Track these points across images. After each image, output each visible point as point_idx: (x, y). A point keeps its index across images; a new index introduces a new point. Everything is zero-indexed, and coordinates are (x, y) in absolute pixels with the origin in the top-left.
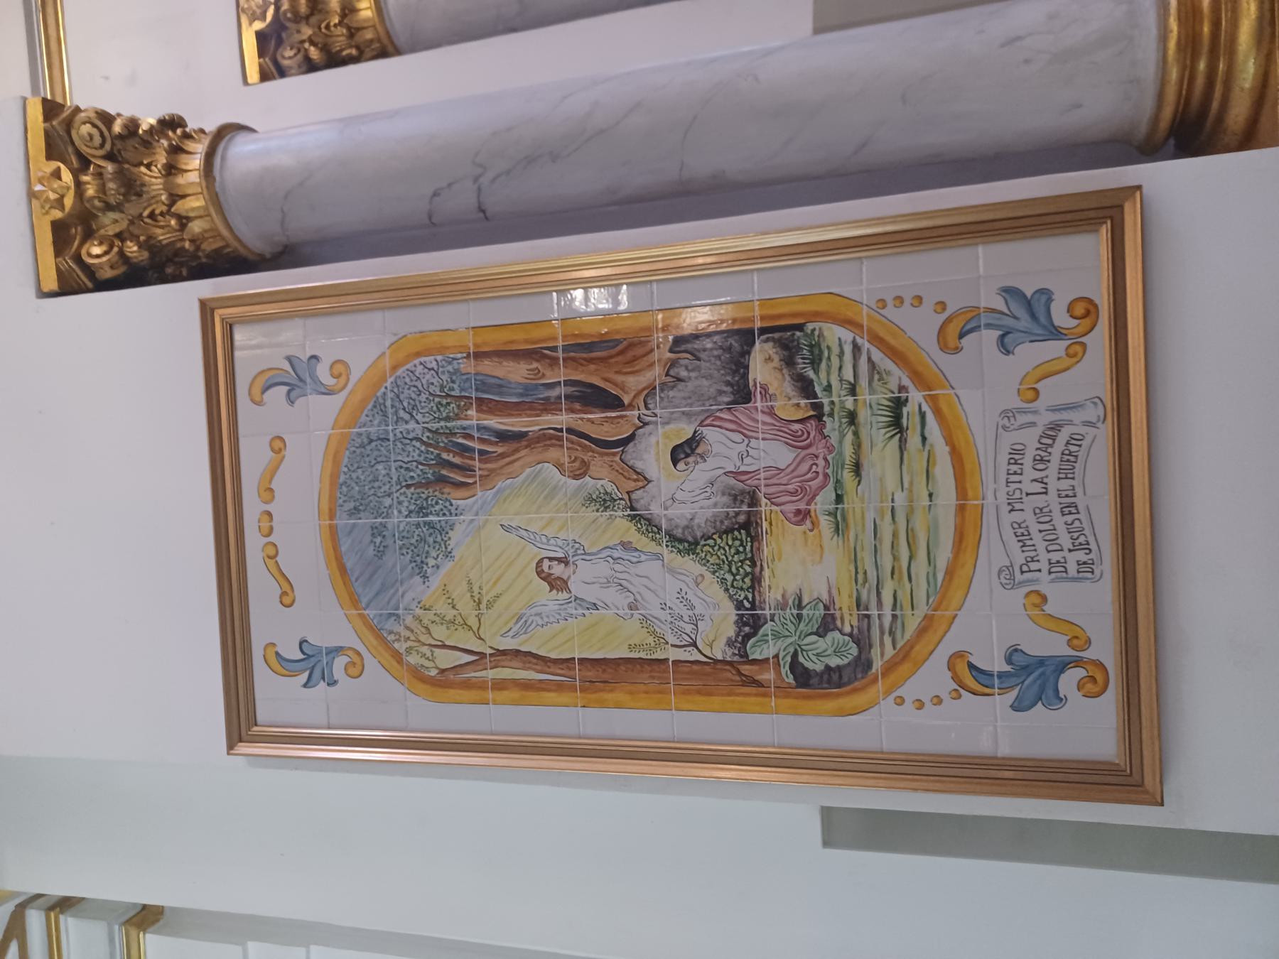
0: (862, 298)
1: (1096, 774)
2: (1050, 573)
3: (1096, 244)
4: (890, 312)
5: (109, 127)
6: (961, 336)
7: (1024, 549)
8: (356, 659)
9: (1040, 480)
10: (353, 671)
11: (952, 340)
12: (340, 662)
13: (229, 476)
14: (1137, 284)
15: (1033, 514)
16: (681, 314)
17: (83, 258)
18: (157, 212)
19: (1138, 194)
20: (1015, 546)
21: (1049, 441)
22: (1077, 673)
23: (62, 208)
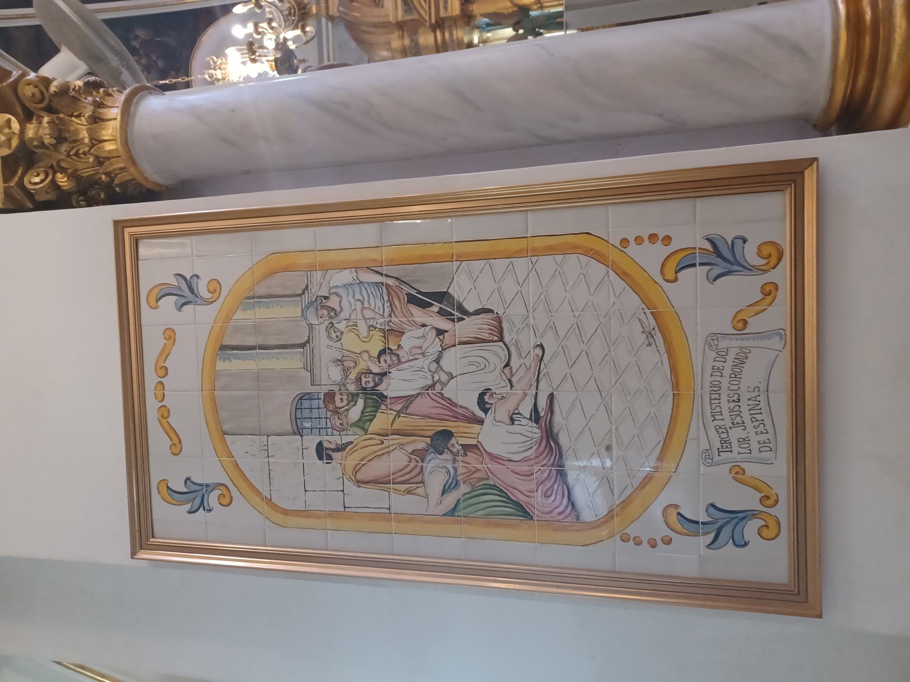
1: (761, 592)
2: (712, 376)
5: (47, 88)
8: (225, 492)
9: (754, 399)
10: (226, 501)
12: (215, 494)
14: (813, 187)
17: (25, 184)
18: (81, 152)
19: (815, 164)
23: (10, 147)
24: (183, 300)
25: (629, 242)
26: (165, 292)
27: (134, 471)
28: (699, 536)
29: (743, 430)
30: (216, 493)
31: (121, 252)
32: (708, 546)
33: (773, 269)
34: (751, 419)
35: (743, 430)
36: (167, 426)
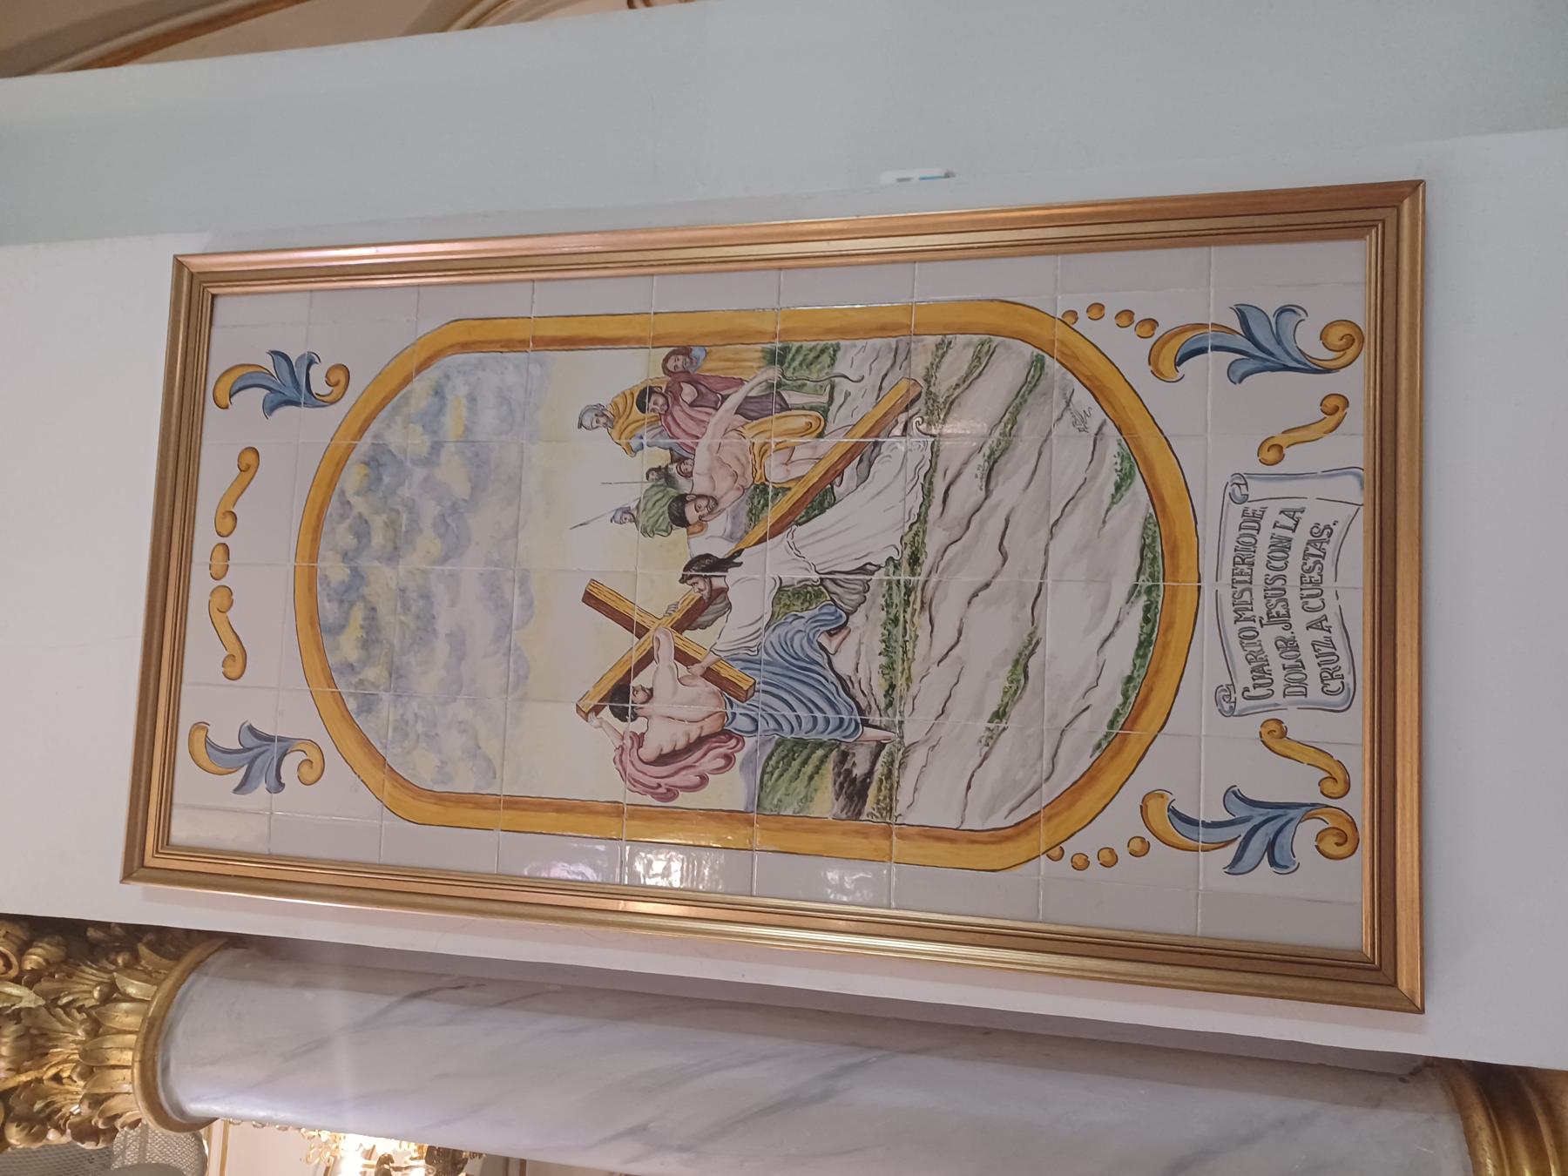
0: (1056, 313)
4: (1083, 324)
6: (1178, 363)
8: (315, 756)
10: (310, 774)
11: (1167, 363)
13: (163, 705)
21: (1280, 564)
24: (279, 398)
25: (1077, 319)
26: (245, 377)
27: (137, 850)
31: (145, 758)
33: (1332, 757)
36: (224, 628)
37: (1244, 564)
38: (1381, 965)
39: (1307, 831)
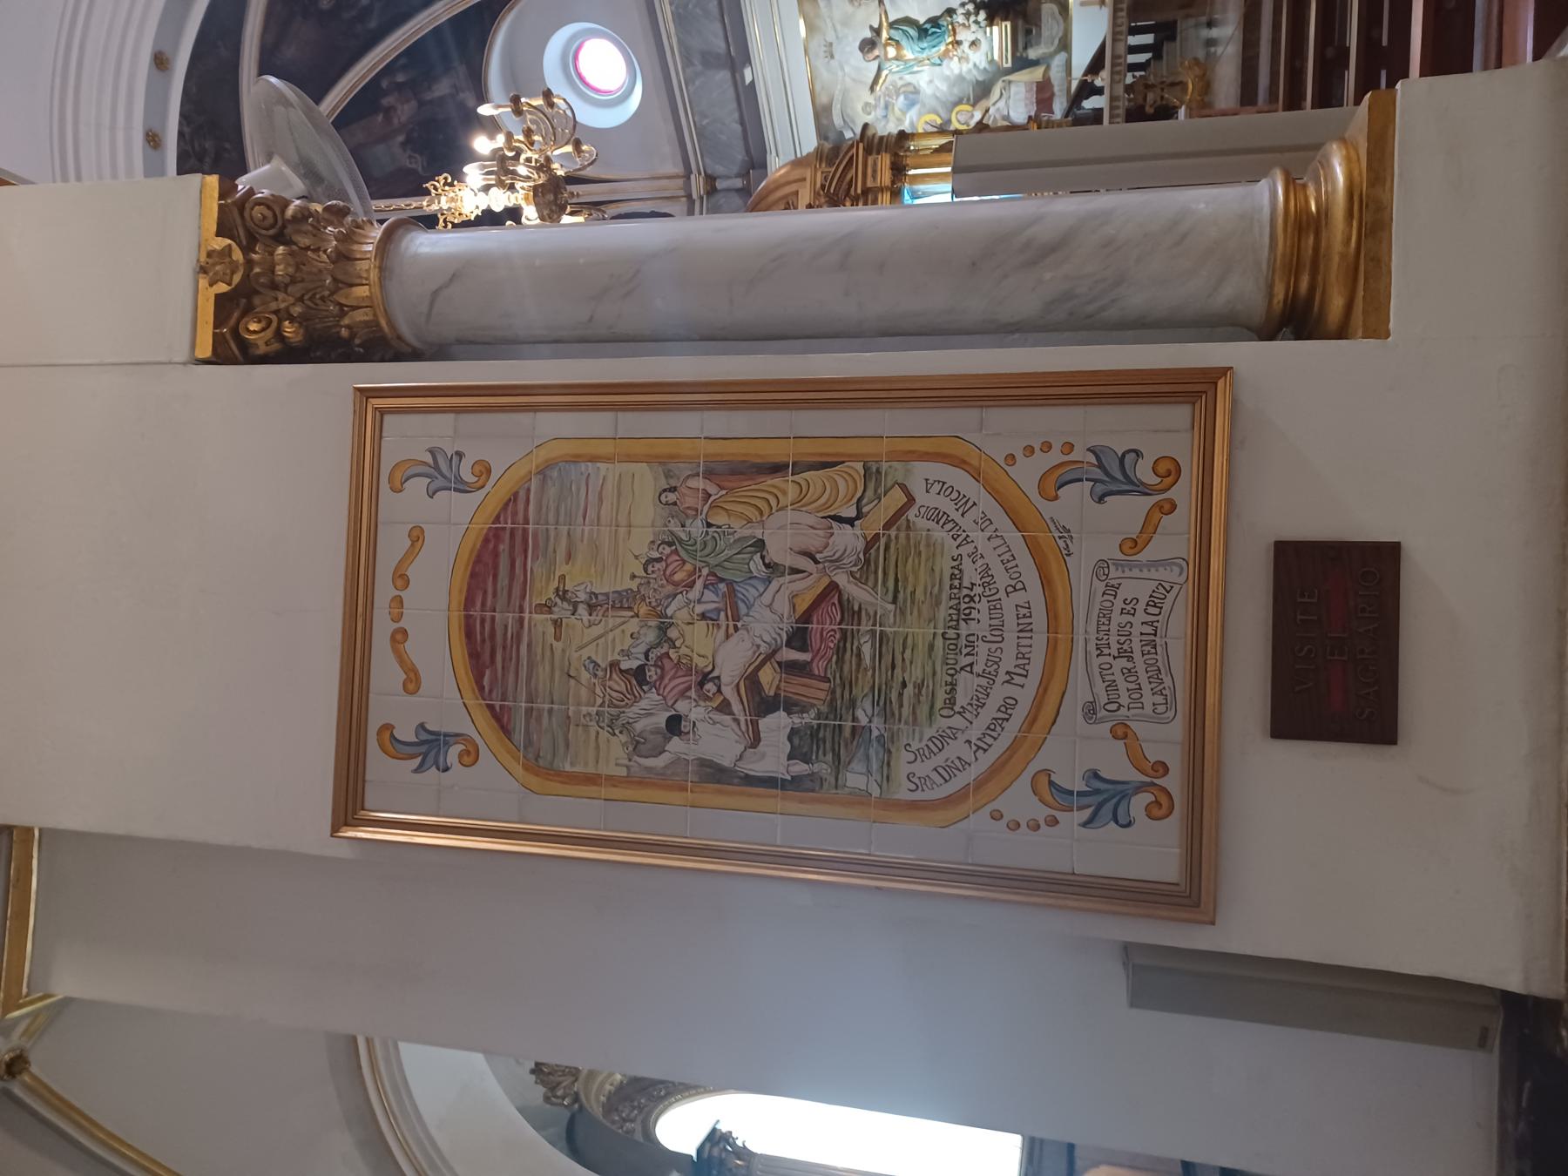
3: (1178, 415)
7: (1108, 689)
10: (466, 760)
15: (1121, 674)
16: (632, 744)
17: (240, 331)
20: (1100, 687)
22: (1144, 798)
28: (1073, 810)
29: (1126, 599)
30: (458, 748)
32: (1085, 825)
34: (1122, 671)
35: (1126, 599)
37: (1104, 617)
38: (1190, 893)
39: (1139, 802)
